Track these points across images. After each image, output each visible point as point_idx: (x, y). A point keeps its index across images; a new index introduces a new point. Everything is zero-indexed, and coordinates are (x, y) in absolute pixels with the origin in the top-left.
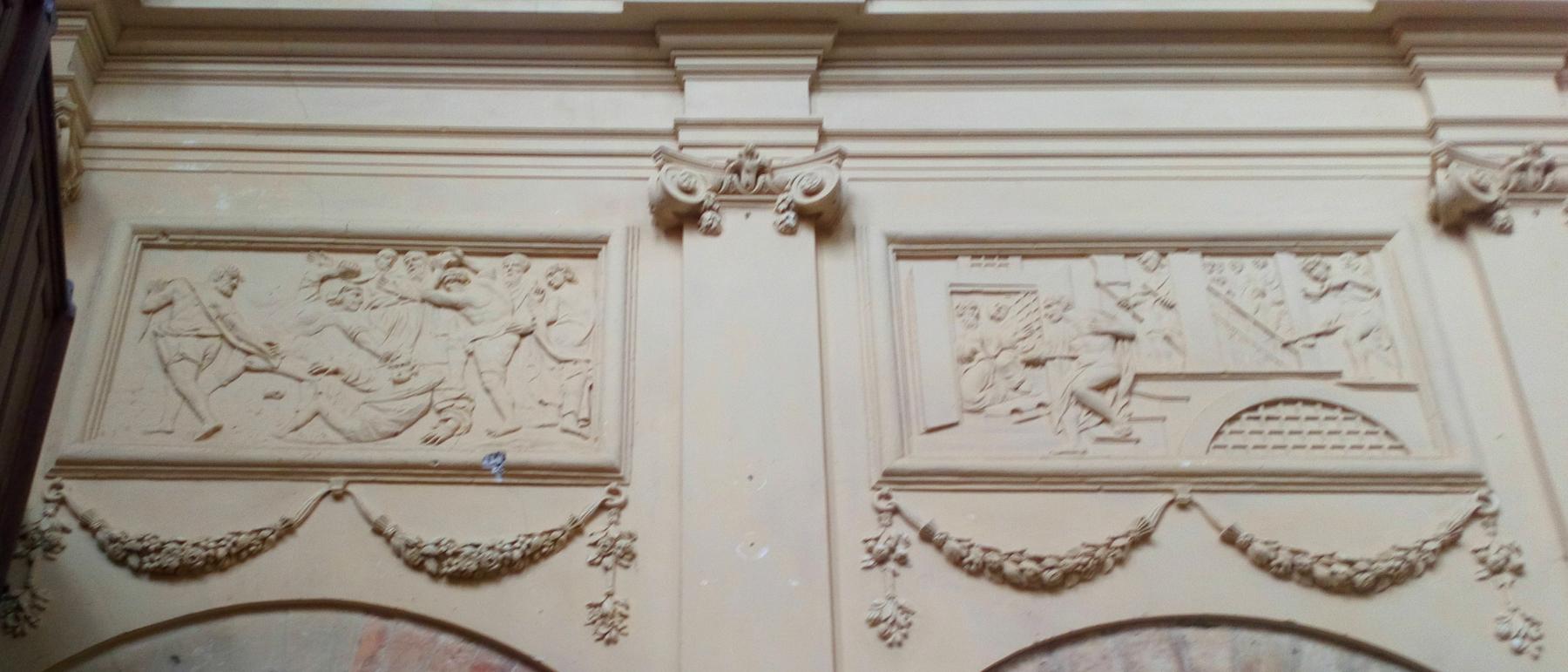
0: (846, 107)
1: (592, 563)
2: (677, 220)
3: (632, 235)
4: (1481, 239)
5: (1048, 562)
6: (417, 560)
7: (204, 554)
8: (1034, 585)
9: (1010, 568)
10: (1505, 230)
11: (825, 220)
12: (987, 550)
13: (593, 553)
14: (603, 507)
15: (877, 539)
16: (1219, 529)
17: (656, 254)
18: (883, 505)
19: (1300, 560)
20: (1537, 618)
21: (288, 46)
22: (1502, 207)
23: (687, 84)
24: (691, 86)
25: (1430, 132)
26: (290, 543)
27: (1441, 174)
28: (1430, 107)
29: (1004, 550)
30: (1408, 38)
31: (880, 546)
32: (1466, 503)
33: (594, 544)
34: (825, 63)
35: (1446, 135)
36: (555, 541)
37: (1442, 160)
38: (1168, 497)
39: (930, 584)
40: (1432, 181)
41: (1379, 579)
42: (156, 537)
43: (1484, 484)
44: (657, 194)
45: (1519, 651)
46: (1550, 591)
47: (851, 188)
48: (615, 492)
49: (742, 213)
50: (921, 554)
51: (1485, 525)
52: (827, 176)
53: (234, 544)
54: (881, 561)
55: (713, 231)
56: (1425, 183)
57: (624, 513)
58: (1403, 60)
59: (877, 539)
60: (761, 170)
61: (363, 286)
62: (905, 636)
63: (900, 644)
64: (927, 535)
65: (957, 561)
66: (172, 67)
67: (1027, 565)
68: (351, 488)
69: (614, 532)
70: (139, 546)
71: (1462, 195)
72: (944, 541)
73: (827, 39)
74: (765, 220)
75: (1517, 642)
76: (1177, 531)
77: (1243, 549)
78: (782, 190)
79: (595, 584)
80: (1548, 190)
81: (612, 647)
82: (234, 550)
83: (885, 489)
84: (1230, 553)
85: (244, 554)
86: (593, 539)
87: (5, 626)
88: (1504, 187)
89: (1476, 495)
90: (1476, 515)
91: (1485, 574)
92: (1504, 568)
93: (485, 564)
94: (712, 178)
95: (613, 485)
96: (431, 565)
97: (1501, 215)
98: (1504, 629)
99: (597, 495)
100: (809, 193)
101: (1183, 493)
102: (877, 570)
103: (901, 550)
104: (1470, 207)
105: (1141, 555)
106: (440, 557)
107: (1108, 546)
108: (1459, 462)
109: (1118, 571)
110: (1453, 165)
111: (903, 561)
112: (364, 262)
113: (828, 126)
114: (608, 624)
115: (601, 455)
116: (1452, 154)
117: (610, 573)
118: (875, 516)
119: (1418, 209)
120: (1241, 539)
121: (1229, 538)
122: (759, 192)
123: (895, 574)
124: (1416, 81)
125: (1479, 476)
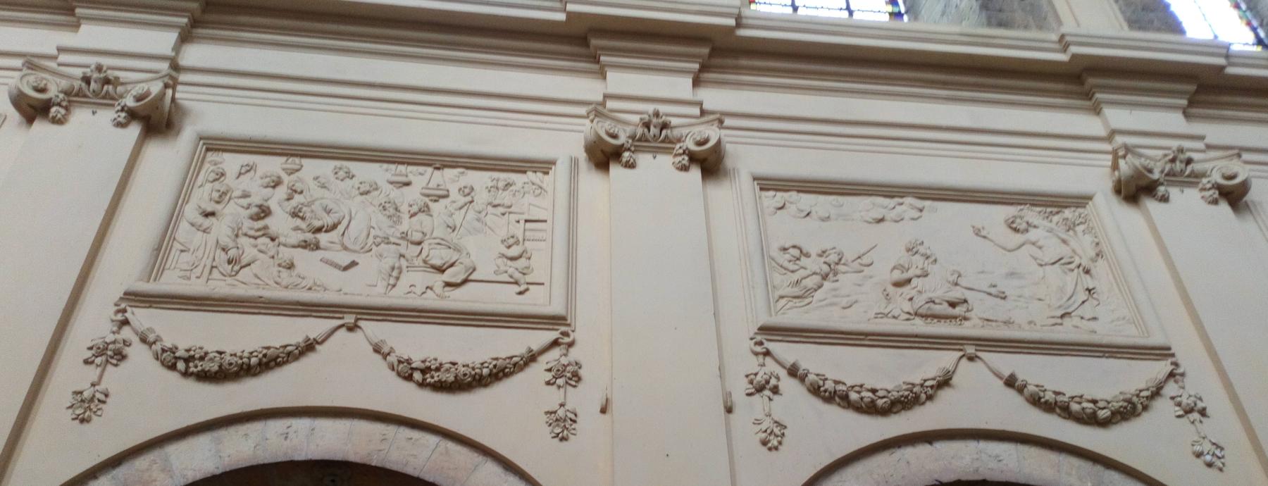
0: (714, 98)
1: (548, 383)
2: (604, 156)
3: (574, 163)
4: (1151, 204)
5: (880, 393)
6: (406, 371)
8: (870, 409)
9: (1075, 407)
10: (1165, 199)
11: (709, 164)
12: (837, 382)
13: (549, 376)
14: (555, 343)
15: (756, 374)
16: (1001, 378)
17: (590, 180)
18: (758, 349)
19: (1060, 398)
20: (1222, 444)
21: (342, 28)
22: (1162, 184)
23: (609, 74)
24: (611, 75)
25: (1109, 138)
26: (310, 359)
28: (1106, 123)
29: (849, 383)
30: (1092, 81)
31: (759, 378)
32: (1163, 367)
33: (550, 370)
34: (704, 68)
35: (1120, 140)
36: (515, 365)
37: (1121, 153)
38: (961, 353)
41: (894, 403)
43: (569, 325)
44: (592, 137)
45: (1210, 465)
47: (729, 148)
48: (565, 334)
50: (789, 385)
51: (1176, 382)
52: (713, 133)
54: (760, 389)
55: (631, 165)
56: (1108, 170)
57: (571, 350)
58: (1088, 96)
59: (756, 374)
60: (107, 81)
62: (780, 443)
63: (776, 448)
64: (793, 371)
65: (815, 390)
66: (234, 33)
67: (1085, 405)
68: (361, 323)
69: (564, 361)
70: (422, 366)
73: (705, 51)
74: (666, 162)
75: (1208, 458)
76: (968, 374)
77: (1020, 390)
78: (679, 140)
79: (552, 397)
80: (1189, 176)
81: (565, 443)
83: (759, 338)
84: (1011, 393)
85: (272, 364)
86: (549, 366)
87: (562, 425)
88: (1162, 172)
90: (1171, 375)
91: (1181, 413)
94: (629, 130)
95: (563, 329)
96: (417, 376)
97: (1161, 189)
98: (1198, 448)
99: (551, 336)
100: (700, 144)
101: (970, 350)
102: (757, 396)
103: (773, 382)
104: (1143, 183)
105: (945, 394)
107: (922, 385)
108: (1156, 339)
109: (928, 403)
110: (1129, 156)
111: (775, 390)
113: (706, 106)
115: (556, 308)
116: (1128, 149)
117: (562, 390)
119: (1109, 185)
120: (801, 372)
121: (1011, 382)
122: (104, 98)
123: (770, 399)
124: (1096, 110)
125: (1169, 349)
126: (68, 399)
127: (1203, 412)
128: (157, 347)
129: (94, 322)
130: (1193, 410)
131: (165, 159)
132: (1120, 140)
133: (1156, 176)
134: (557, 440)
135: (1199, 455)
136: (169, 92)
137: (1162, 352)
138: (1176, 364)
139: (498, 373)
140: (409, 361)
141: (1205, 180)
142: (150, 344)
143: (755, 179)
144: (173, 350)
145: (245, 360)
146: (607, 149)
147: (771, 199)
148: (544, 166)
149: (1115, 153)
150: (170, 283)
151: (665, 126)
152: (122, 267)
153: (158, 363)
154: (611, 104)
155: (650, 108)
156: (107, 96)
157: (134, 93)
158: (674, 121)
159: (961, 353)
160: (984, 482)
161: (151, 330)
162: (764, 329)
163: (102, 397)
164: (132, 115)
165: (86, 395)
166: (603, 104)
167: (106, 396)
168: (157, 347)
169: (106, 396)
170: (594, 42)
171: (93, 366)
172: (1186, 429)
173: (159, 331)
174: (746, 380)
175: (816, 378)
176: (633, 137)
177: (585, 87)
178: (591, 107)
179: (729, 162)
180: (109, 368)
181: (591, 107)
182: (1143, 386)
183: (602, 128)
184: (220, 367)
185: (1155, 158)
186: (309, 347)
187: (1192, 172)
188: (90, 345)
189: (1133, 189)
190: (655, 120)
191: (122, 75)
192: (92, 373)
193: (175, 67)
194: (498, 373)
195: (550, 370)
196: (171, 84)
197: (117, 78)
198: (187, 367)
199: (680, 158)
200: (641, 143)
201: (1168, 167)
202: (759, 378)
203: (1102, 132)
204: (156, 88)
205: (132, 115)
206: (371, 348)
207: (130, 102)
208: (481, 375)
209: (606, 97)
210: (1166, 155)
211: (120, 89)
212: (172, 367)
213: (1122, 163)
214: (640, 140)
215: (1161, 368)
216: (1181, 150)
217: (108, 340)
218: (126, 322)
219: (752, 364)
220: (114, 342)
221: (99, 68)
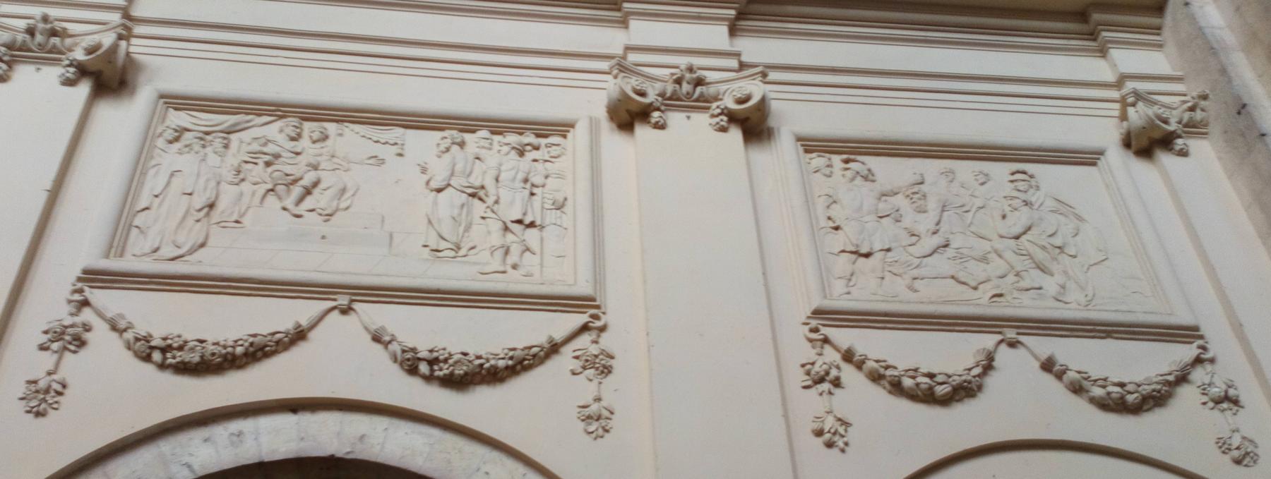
0: (756, 48)
2: (629, 115)
7: (224, 351)
10: (1183, 153)
11: (753, 125)
14: (585, 328)
15: (813, 364)
17: (612, 140)
22: (1180, 137)
25: (1118, 84)
27: (1131, 110)
31: (817, 368)
34: (741, 15)
35: (1130, 85)
36: (534, 356)
37: (1131, 100)
38: (999, 337)
39: (859, 395)
40: (1124, 117)
42: (179, 336)
46: (1259, 419)
47: (775, 106)
49: (683, 115)
50: (849, 374)
52: (757, 90)
53: (511, 358)
55: (661, 126)
57: (604, 335)
58: (1092, 35)
59: (813, 364)
60: (54, 33)
61: (233, 137)
64: (848, 356)
66: (1137, 36)
68: (356, 306)
69: (594, 350)
70: (162, 344)
71: (1151, 125)
72: (863, 362)
74: (702, 121)
77: (1059, 376)
78: (716, 99)
79: (585, 389)
81: (41, 419)
82: (251, 349)
83: (814, 323)
84: (1048, 379)
85: (519, 367)
88: (1179, 122)
89: (1195, 345)
90: (1198, 361)
91: (809, 383)
92: (1228, 400)
93: (207, 356)
94: (659, 86)
96: (157, 356)
99: (579, 319)
100: (90, 51)
101: (1011, 334)
103: (834, 373)
104: (1157, 135)
106: (432, 362)
110: (1140, 104)
111: (837, 383)
112: (331, 128)
114: (596, 420)
115: (583, 288)
116: (1138, 96)
118: (809, 345)
120: (1057, 368)
121: (1048, 366)
122: (697, 100)
124: (1103, 52)
125: (1196, 329)
126: (21, 390)
127: (1236, 402)
128: (129, 335)
129: (48, 303)
130: (1228, 400)
131: (121, 121)
132: (1130, 85)
133: (1172, 127)
134: (31, 415)
135: (819, 433)
136: (123, 44)
137: (1187, 333)
138: (1204, 348)
139: (520, 365)
140: (414, 350)
141: (714, 105)
142: (121, 332)
143: (799, 139)
144: (147, 339)
145: (230, 350)
146: (634, 108)
147: (818, 161)
148: (562, 128)
149: (1123, 102)
150: (127, 264)
151: (699, 82)
152: (78, 244)
153: (130, 353)
154: (633, 57)
155: (683, 61)
156: (54, 50)
157: (84, 44)
158: (711, 76)
159: (999, 337)
160: (332, 456)
161: (122, 316)
162: (818, 313)
163: (59, 388)
164: (83, 71)
165: (42, 384)
166: (624, 58)
167: (64, 386)
168: (129, 335)
169: (64, 386)
170: (1096, 16)
171: (47, 353)
172: (1219, 421)
173: (130, 318)
174: (802, 370)
175: (875, 365)
176: (662, 95)
177: (609, 39)
178: (613, 62)
179: (772, 122)
180: (68, 355)
181: (613, 62)
182: (970, 364)
183: (629, 84)
184: (202, 357)
185: (1172, 105)
186: (299, 335)
187: (702, 95)
188: (45, 328)
189: (1144, 142)
190: (688, 76)
191: (72, 28)
192: (48, 360)
193: (127, 16)
194: (520, 365)
195: (46, 332)
196: (125, 34)
197: (65, 29)
198: (432, 371)
199: (717, 119)
200: (672, 101)
201: (1186, 116)
202: (817, 368)
203: (1110, 77)
204: (108, 40)
205: (83, 71)
206: (368, 337)
207: (79, 55)
208: (233, 355)
209: (628, 49)
210: (673, 74)
211: (68, 41)
212: (147, 358)
213: (1131, 110)
214: (670, 99)
215: (1186, 352)
216: (691, 69)
217: (66, 323)
218: (86, 303)
219: (809, 353)
220: (72, 326)
221: (45, 19)
